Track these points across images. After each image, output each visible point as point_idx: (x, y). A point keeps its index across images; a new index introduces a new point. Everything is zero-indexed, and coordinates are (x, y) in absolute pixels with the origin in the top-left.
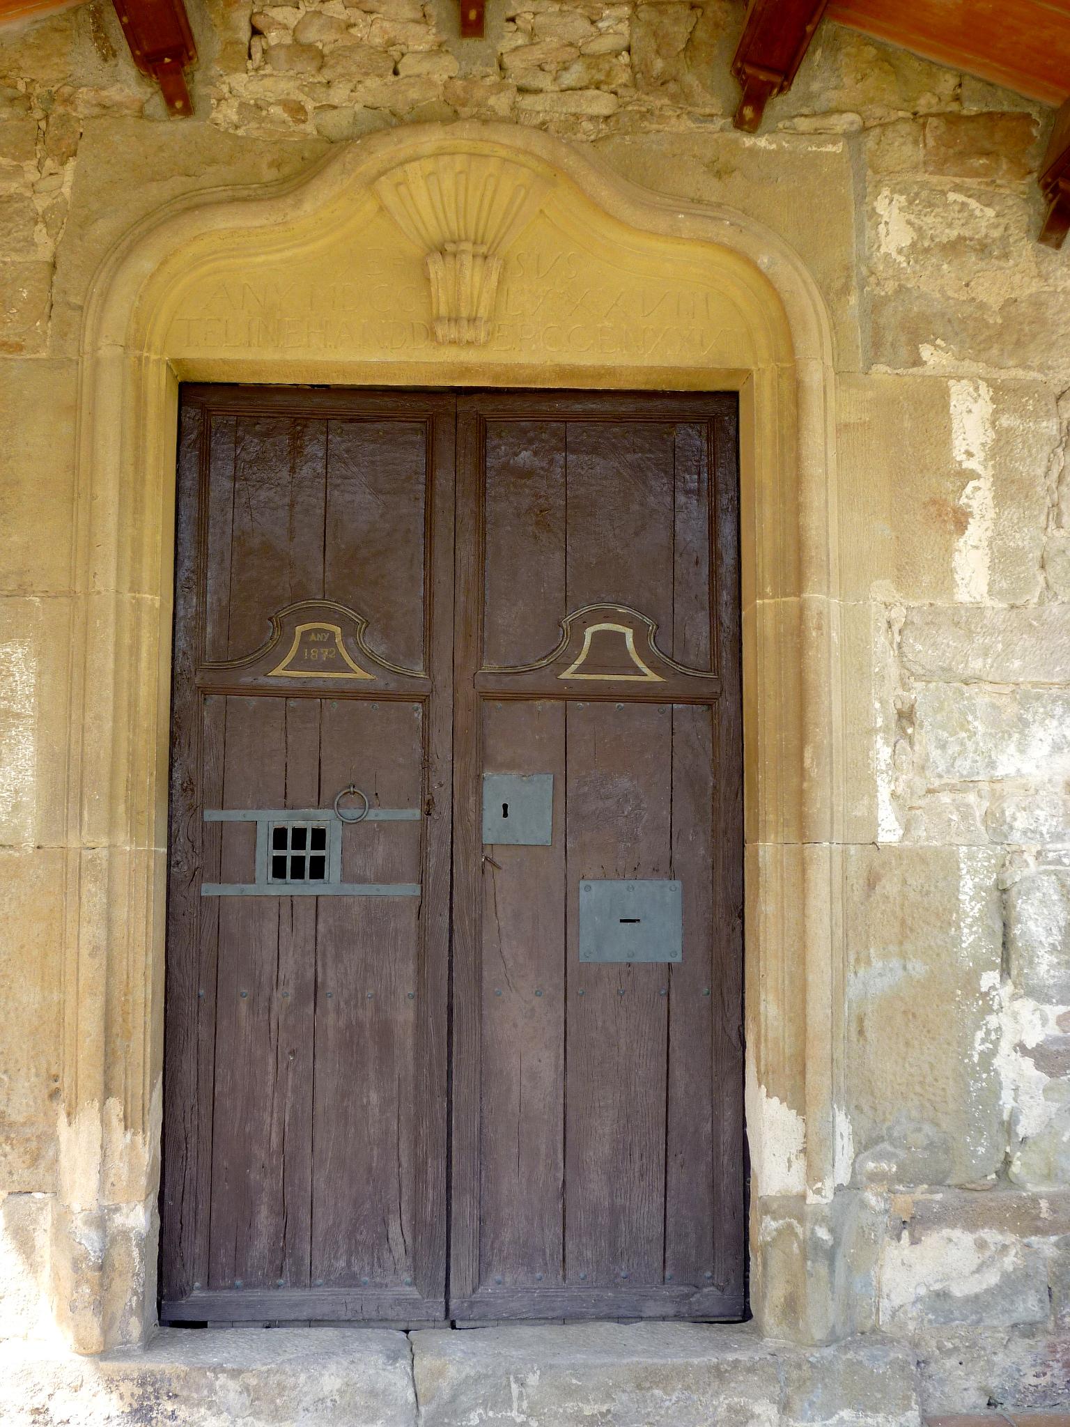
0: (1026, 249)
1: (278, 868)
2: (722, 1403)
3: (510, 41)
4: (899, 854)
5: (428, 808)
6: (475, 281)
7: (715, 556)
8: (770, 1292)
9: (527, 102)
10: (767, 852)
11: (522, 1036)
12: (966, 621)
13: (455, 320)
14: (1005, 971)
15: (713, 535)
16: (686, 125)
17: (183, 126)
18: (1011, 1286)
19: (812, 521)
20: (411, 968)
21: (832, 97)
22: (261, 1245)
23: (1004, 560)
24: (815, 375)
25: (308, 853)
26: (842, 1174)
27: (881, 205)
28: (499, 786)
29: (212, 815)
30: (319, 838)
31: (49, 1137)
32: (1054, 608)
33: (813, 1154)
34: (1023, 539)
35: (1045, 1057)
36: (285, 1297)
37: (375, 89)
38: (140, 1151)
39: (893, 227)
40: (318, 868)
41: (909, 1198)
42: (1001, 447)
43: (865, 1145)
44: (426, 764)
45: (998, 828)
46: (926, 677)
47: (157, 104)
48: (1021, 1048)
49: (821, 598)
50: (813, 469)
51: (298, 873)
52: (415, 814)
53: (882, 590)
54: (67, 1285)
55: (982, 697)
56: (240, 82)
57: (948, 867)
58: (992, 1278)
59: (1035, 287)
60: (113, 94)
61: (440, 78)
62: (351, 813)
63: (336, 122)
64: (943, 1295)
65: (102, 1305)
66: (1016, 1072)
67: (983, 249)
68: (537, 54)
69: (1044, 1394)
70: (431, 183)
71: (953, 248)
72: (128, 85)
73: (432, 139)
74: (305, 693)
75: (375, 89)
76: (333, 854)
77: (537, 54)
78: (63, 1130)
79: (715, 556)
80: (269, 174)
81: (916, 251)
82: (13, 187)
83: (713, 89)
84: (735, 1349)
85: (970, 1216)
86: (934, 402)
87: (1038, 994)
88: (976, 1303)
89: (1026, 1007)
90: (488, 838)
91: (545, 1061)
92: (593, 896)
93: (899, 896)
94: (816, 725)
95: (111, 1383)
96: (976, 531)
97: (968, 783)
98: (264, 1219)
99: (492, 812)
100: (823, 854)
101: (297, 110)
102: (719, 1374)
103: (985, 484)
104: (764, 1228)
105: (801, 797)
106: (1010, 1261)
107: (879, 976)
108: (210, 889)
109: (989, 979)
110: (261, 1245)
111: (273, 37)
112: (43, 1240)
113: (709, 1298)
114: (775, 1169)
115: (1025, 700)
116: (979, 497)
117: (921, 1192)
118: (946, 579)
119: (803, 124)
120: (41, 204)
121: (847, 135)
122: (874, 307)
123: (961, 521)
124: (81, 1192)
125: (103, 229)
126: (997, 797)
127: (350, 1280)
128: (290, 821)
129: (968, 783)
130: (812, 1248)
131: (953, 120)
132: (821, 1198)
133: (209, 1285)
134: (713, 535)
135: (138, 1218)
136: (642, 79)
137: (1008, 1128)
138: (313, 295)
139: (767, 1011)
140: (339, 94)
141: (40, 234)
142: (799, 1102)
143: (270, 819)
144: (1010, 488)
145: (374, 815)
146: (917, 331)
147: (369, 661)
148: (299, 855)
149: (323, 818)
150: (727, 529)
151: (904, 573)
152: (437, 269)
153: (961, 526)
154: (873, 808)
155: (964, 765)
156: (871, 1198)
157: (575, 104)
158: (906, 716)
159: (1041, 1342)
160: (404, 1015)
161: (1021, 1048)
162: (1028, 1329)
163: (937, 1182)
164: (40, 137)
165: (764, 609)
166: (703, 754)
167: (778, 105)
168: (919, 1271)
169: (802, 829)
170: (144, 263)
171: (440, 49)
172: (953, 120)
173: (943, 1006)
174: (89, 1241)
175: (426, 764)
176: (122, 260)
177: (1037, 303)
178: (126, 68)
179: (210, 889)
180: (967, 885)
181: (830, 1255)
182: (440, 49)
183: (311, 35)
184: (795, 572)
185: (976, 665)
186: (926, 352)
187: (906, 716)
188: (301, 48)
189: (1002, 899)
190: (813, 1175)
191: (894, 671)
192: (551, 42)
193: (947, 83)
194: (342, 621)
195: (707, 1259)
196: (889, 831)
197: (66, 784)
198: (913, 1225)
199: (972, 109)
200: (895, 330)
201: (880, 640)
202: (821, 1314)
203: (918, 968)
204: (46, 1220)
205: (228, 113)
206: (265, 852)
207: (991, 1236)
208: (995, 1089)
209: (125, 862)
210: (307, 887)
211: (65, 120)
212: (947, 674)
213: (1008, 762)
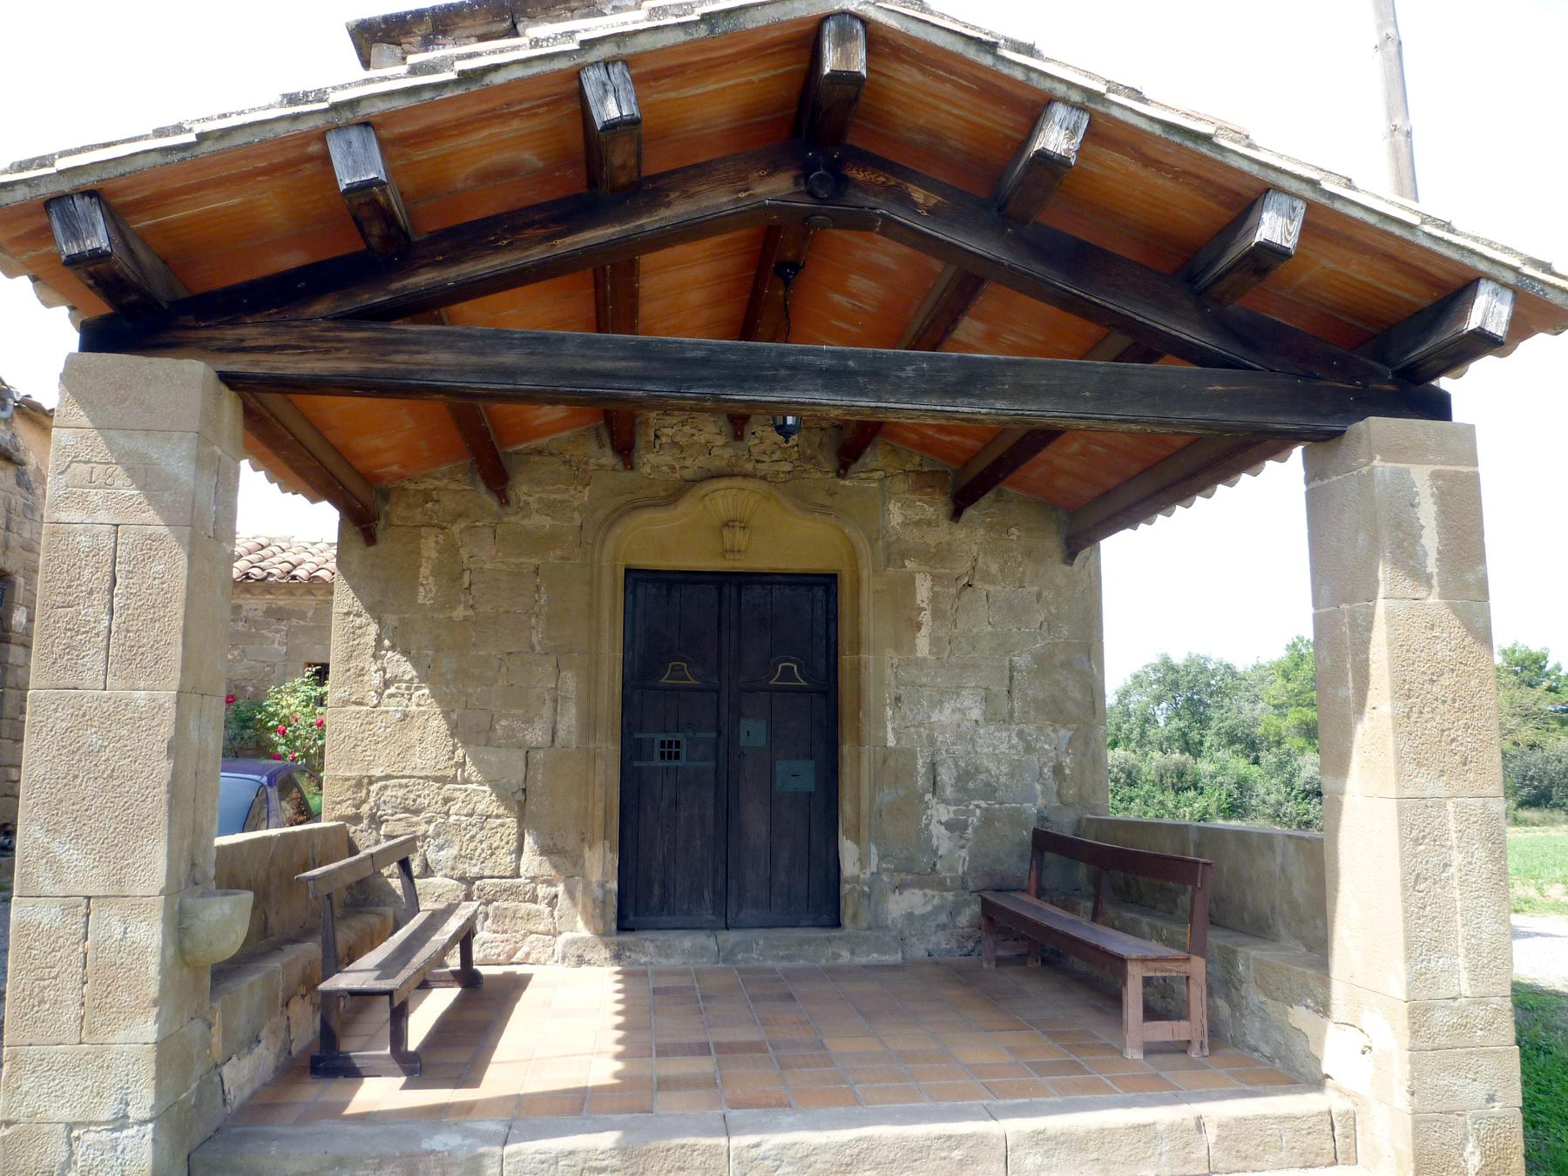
0: (945, 523)
1: (662, 756)
2: (830, 951)
3: (752, 442)
4: (894, 750)
5: (719, 733)
6: (740, 538)
7: (828, 638)
8: (846, 920)
9: (759, 466)
10: (846, 749)
11: (755, 821)
12: (920, 664)
13: (732, 551)
14: (934, 794)
15: (827, 630)
16: (819, 475)
17: (631, 474)
18: (937, 911)
19: (864, 629)
20: (712, 793)
21: (874, 465)
22: (655, 900)
23: (935, 641)
24: (865, 574)
25: (674, 750)
26: (874, 869)
27: (891, 507)
28: (747, 725)
29: (637, 735)
30: (678, 744)
31: (581, 856)
32: (953, 659)
33: (863, 861)
34: (941, 633)
35: (948, 825)
36: (665, 919)
37: (702, 460)
38: (613, 859)
39: (896, 515)
40: (677, 756)
41: (898, 878)
42: (935, 598)
43: (882, 858)
44: (718, 717)
45: (932, 741)
46: (905, 685)
47: (620, 466)
48: (940, 822)
49: (867, 657)
50: (864, 609)
51: (670, 757)
52: (714, 735)
53: (889, 653)
54: (590, 910)
55: (926, 692)
56: (651, 457)
57: (913, 756)
58: (929, 908)
59: (948, 538)
60: (603, 461)
61: (727, 456)
62: (690, 735)
63: (688, 474)
64: (911, 914)
65: (603, 916)
66: (938, 831)
67: (929, 523)
68: (763, 447)
69: (949, 951)
70: (723, 499)
71: (918, 523)
72: (608, 458)
73: (724, 483)
74: (673, 688)
75: (702, 460)
76: (683, 751)
77: (763, 447)
78: (587, 853)
79: (828, 638)
80: (663, 494)
81: (904, 524)
82: (566, 497)
83: (829, 462)
84: (835, 933)
85: (922, 885)
86: (909, 582)
87: (946, 802)
88: (924, 917)
89: (941, 807)
90: (742, 744)
91: (763, 829)
92: (781, 766)
93: (895, 765)
94: (1423, 527)
95: (606, 946)
96: (924, 631)
97: (921, 724)
98: (657, 889)
99: (743, 736)
100: (866, 750)
101: (673, 468)
102: (829, 940)
103: (928, 613)
104: (845, 888)
105: (858, 730)
106: (936, 901)
107: (887, 795)
108: (636, 764)
109: (928, 796)
110: (655, 900)
111: (664, 440)
112: (579, 895)
113: (825, 918)
114: (849, 867)
115: (942, 693)
116: (926, 617)
117: (903, 876)
118: (913, 648)
119: (862, 475)
120: (576, 503)
121: (879, 480)
122: (889, 545)
123: (919, 626)
124: (595, 875)
125: (601, 514)
126: (932, 730)
127: (689, 913)
128: (667, 737)
129: (921, 724)
130: (863, 894)
131: (919, 474)
132: (866, 876)
133: (636, 914)
134: (827, 630)
135: (614, 885)
136: (803, 457)
137: (935, 852)
138: (678, 539)
139: (846, 808)
140: (688, 463)
141: (576, 515)
142: (857, 841)
143: (659, 737)
144: (937, 614)
145: (699, 735)
146: (904, 555)
147: (696, 677)
148: (670, 751)
149: (679, 736)
150: (832, 627)
151: (897, 646)
152: (726, 532)
153: (919, 629)
154: (885, 733)
155: (919, 717)
156: (885, 878)
157: (777, 467)
158: (898, 699)
159: (948, 932)
160: (710, 812)
161: (940, 822)
162: (943, 927)
163: (909, 872)
164: (576, 477)
165: (845, 659)
166: (821, 711)
167: (854, 468)
168: (903, 904)
169: (859, 742)
170: (618, 530)
171: (725, 446)
172: (919, 474)
173: (912, 806)
174: (599, 893)
175: (718, 717)
176: (611, 526)
177: (949, 544)
178: (608, 451)
179: (636, 764)
180: (920, 762)
181: (869, 897)
182: (725, 446)
183: (677, 439)
184: (857, 646)
185: (924, 680)
186: (907, 563)
187: (898, 699)
188: (674, 444)
189: (933, 767)
190: (863, 867)
191: (893, 683)
192: (768, 442)
193: (917, 459)
194: (687, 661)
195: (821, 901)
196: (891, 741)
197: (589, 724)
198: (900, 887)
199: (926, 469)
200: (895, 554)
201: (888, 671)
202: (865, 918)
203: (902, 792)
204: (580, 887)
205: (646, 470)
206: (657, 749)
207: (929, 892)
208: (930, 836)
209: (609, 748)
210: (673, 763)
211: (585, 471)
212: (913, 684)
213: (936, 717)
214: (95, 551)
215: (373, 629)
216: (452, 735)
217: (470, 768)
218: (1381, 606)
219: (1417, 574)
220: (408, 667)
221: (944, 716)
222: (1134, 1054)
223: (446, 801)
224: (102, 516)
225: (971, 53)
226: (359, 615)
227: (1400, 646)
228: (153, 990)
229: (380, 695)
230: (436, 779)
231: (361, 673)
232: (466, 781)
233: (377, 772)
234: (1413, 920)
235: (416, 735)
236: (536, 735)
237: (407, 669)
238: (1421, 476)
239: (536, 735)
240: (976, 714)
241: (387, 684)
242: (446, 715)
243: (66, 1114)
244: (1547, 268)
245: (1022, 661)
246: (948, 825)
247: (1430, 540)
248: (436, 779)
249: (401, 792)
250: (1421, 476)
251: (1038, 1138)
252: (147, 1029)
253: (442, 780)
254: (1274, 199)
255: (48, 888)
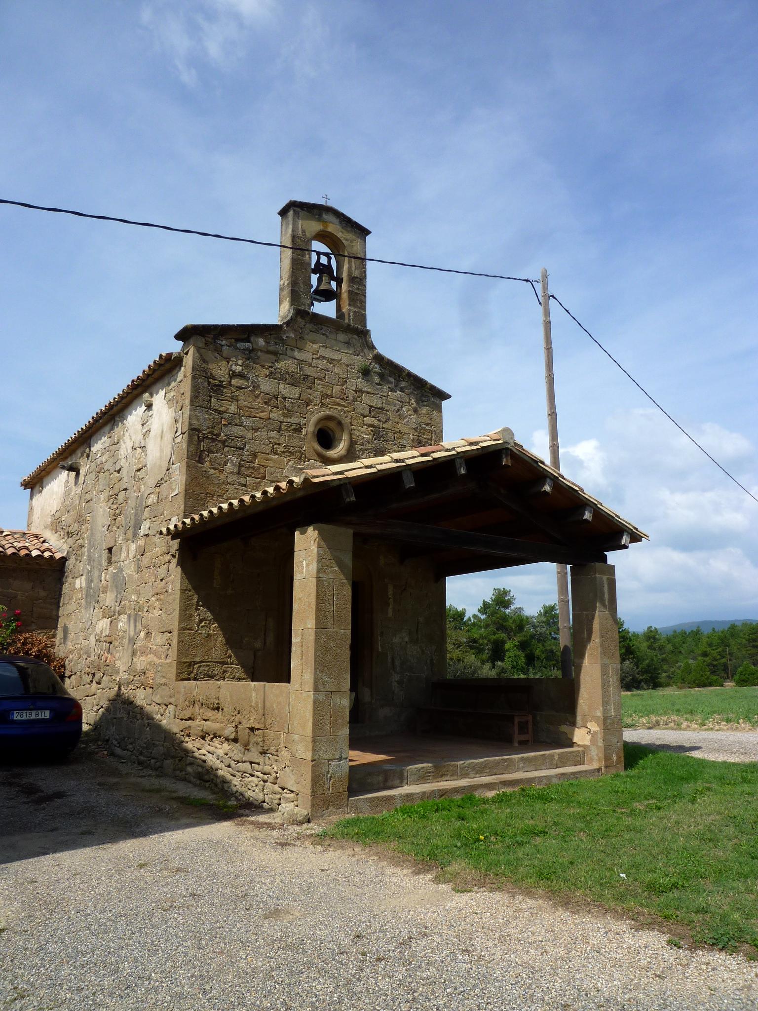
35: (398, 682)
66: (395, 684)
116: (391, 601)
168: (385, 712)
196: (380, 650)
214: (329, 587)
215: (196, 597)
216: (227, 644)
217: (233, 658)
218: (597, 613)
219: (604, 606)
220: (210, 614)
221: (396, 640)
222: (516, 744)
223: (224, 672)
224: (330, 576)
225: (532, 463)
226: (190, 591)
227: (601, 624)
228: (348, 719)
229: (198, 626)
230: (220, 663)
231: (191, 616)
232: (232, 664)
233: (198, 660)
234: (604, 696)
235: (213, 644)
236: (258, 645)
237: (209, 615)
238: (605, 578)
239: (258, 645)
240: (406, 639)
241: (201, 621)
242: (224, 635)
243: (327, 757)
244: (636, 529)
245: (421, 619)
246: (398, 682)
247: (606, 596)
248: (220, 663)
249: (206, 669)
250: (605, 578)
251: (522, 759)
252: (346, 731)
253: (223, 663)
254: (588, 508)
255: (322, 689)
